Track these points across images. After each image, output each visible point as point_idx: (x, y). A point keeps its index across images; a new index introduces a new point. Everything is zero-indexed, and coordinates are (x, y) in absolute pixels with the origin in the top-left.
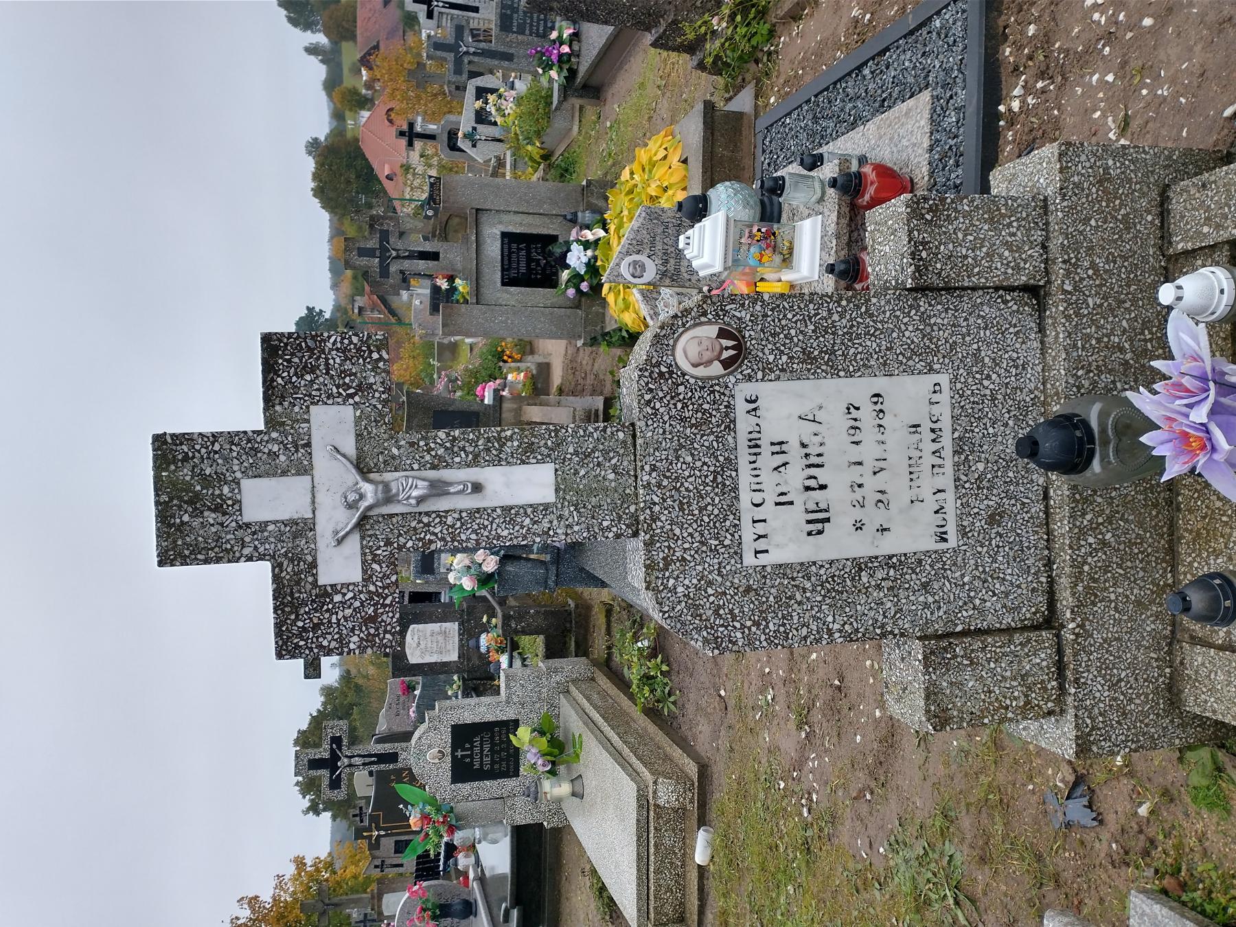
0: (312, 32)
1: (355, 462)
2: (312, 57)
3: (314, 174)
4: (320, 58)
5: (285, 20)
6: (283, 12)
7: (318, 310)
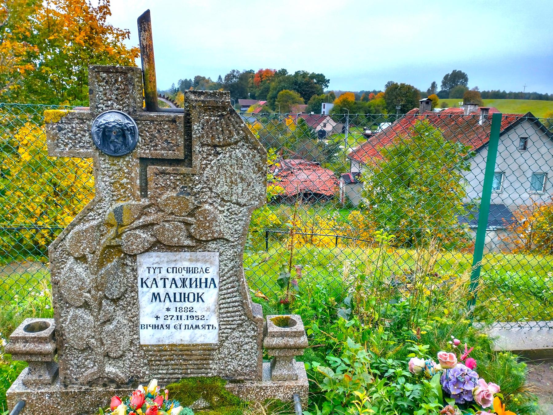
0: (441, 86)
1: (485, 153)
2: (431, 85)
3: (404, 84)
4: (430, 89)
5: (447, 73)
6: (450, 73)
7: (328, 85)
